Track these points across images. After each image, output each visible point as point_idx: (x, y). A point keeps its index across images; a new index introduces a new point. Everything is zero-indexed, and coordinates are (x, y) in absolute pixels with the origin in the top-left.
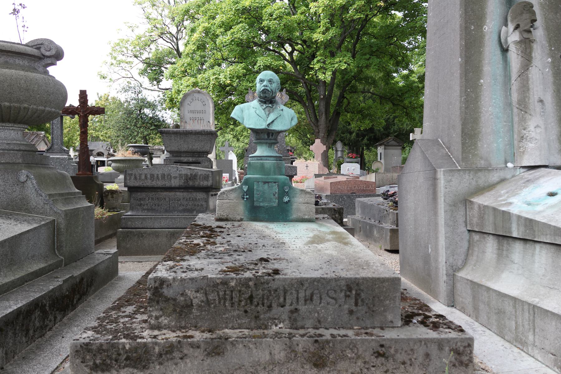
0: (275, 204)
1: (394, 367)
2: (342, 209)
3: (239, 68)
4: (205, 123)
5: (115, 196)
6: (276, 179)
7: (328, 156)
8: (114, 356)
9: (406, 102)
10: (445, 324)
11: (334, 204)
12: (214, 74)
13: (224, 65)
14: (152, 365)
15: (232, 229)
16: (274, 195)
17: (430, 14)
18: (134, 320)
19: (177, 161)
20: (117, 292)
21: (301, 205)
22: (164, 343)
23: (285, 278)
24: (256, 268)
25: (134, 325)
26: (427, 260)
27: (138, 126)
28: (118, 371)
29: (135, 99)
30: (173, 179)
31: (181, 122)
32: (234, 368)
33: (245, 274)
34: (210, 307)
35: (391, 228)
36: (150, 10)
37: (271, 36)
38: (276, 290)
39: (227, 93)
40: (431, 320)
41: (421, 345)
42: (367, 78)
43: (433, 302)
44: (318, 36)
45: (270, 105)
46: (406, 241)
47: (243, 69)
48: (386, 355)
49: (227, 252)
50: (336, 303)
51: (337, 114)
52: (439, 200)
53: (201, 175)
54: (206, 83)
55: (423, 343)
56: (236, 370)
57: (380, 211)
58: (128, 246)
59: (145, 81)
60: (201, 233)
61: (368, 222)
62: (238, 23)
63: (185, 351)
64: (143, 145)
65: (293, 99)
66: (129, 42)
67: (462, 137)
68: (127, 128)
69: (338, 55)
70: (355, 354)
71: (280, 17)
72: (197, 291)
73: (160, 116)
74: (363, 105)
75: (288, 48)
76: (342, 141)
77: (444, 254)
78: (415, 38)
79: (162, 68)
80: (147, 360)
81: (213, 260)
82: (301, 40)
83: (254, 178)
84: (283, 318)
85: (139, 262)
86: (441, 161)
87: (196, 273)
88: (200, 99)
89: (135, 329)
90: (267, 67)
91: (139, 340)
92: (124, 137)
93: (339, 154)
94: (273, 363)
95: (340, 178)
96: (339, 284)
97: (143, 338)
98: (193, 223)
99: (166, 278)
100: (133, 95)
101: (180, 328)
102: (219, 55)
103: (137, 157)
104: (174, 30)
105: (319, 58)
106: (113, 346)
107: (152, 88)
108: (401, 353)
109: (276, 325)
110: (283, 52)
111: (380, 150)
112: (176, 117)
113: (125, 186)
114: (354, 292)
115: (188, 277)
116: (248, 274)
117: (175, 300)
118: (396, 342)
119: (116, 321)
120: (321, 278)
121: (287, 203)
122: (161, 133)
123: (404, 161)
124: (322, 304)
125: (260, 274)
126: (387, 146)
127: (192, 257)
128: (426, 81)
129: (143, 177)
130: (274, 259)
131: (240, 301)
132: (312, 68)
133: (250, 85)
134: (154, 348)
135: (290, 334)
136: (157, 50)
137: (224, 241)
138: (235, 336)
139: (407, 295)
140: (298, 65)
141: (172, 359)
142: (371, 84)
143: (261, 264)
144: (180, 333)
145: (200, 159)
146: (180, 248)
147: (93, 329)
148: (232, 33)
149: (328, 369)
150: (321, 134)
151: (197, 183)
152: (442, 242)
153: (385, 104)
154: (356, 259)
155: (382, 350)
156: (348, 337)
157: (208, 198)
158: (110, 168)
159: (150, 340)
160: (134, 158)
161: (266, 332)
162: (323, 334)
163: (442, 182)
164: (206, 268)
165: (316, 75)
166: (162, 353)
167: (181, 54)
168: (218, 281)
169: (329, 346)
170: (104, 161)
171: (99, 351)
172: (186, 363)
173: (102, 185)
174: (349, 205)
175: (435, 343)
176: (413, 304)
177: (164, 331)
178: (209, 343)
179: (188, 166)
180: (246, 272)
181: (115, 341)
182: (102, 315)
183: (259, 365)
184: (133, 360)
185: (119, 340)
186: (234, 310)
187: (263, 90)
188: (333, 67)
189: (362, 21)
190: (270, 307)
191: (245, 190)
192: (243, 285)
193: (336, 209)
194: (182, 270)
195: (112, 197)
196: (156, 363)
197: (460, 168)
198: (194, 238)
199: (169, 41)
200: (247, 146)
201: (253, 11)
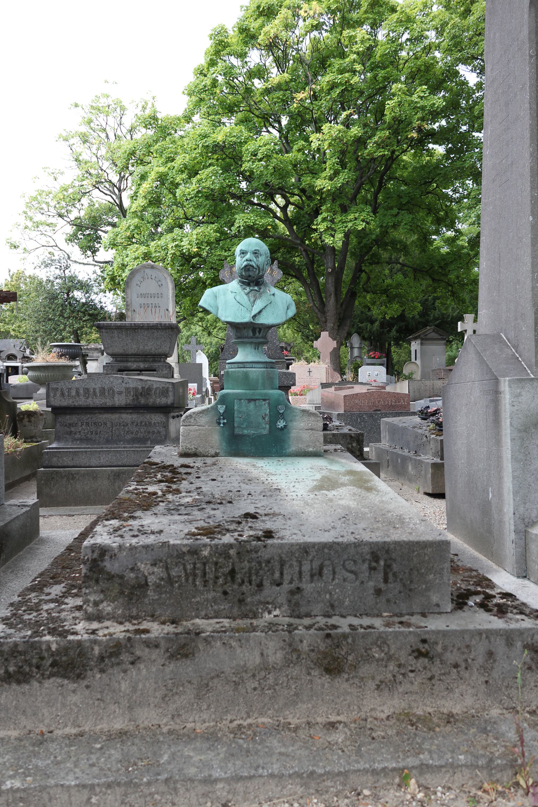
0: (265, 432)
1: (443, 671)
2: (362, 435)
3: (210, 231)
4: (162, 313)
5: (33, 419)
6: (266, 394)
7: (339, 356)
8: (34, 661)
9: (452, 276)
10: (516, 608)
11: (350, 427)
12: (174, 240)
13: (188, 228)
14: (89, 673)
15: (203, 469)
17: (486, 152)
18: (63, 606)
19: (122, 368)
20: (38, 563)
22: (107, 641)
23: (282, 544)
24: (239, 529)
25: (63, 614)
26: (486, 509)
27: (65, 315)
28: (40, 682)
29: (61, 278)
30: (116, 395)
31: (127, 310)
32: (209, 677)
33: (223, 538)
34: (173, 587)
35: (433, 461)
36: (79, 147)
37: (255, 184)
38: (268, 562)
39: (193, 266)
40: (495, 601)
41: (481, 639)
42: (394, 243)
43: (496, 571)
44: (322, 183)
45: (256, 288)
46: (455, 481)
47: (216, 231)
48: (431, 655)
49: (196, 505)
50: (357, 579)
51: (352, 295)
52: (503, 424)
53: (157, 389)
55: (484, 636)
56: (212, 678)
57: (416, 437)
58: (53, 492)
59: (75, 251)
60: (159, 476)
61: (400, 452)
62: (205, 167)
63: (138, 653)
64: (73, 343)
65: (289, 274)
66: (51, 195)
67: (535, 331)
68: (50, 320)
69: (352, 209)
70: (386, 654)
71: (268, 157)
72: (154, 565)
73: (96, 301)
74: (389, 281)
75: (279, 199)
76: (359, 334)
77: (512, 502)
78: (463, 184)
79: (99, 232)
80: (83, 667)
81: (177, 517)
82: (299, 189)
83: (233, 394)
84: (279, 601)
85: (70, 515)
86: (505, 366)
87: (152, 537)
89: (65, 620)
90: (249, 231)
91: (71, 637)
92: (45, 331)
93: (356, 352)
94: (265, 667)
95: (358, 389)
96: (360, 551)
97: (76, 633)
98: (146, 460)
99: (109, 546)
100: (58, 272)
101: (130, 618)
102: (180, 213)
103: (64, 362)
104: (115, 179)
105: (325, 215)
106: (33, 646)
107: (85, 261)
108: (451, 651)
109: (270, 613)
110: (273, 206)
111: (415, 346)
112: (119, 301)
113: (48, 406)
114: (382, 563)
115: (141, 543)
116: (227, 539)
117: (122, 577)
118: (444, 635)
119: (37, 608)
120: (334, 543)
121: (282, 429)
122: (100, 328)
123: (451, 361)
124: (337, 581)
125: (244, 538)
126: (424, 340)
128: (481, 244)
129: (73, 393)
130: (266, 515)
131: (217, 578)
132: (316, 230)
133: (226, 254)
134: (93, 649)
135: (290, 625)
136: (91, 205)
138: (210, 629)
139: (460, 564)
140: (295, 224)
141: (118, 664)
142: (401, 250)
143: (247, 522)
144: (130, 625)
145: (156, 365)
146: (130, 500)
147: (3, 620)
148: (199, 181)
149: (346, 676)
150: (330, 325)
151: (151, 400)
152: (508, 483)
153: (421, 279)
154: (383, 512)
155: (424, 648)
156: (374, 628)
157: (168, 421)
158: (26, 377)
159: (86, 636)
160: (60, 364)
161: (255, 622)
162: (337, 624)
163: (508, 396)
164: (167, 529)
165: (320, 238)
166: (104, 655)
167: (126, 211)
168: (185, 549)
169: (348, 643)
170: (17, 367)
171: (12, 654)
172: (139, 669)
173: (15, 404)
174: (372, 428)
175: (501, 635)
176: (468, 577)
177: (107, 623)
178: (173, 640)
179: (139, 375)
180: (225, 535)
181: (36, 639)
182: (16, 599)
183: (246, 671)
184: (61, 666)
185: (41, 637)
186: (208, 591)
187: (245, 266)
189: (387, 160)
190: (260, 586)
191: (222, 411)
192: (220, 555)
193: (353, 435)
194: (132, 533)
195: (30, 421)
196: (96, 670)
197: (533, 376)
198: (149, 483)
199: (108, 193)
201: (229, 148)
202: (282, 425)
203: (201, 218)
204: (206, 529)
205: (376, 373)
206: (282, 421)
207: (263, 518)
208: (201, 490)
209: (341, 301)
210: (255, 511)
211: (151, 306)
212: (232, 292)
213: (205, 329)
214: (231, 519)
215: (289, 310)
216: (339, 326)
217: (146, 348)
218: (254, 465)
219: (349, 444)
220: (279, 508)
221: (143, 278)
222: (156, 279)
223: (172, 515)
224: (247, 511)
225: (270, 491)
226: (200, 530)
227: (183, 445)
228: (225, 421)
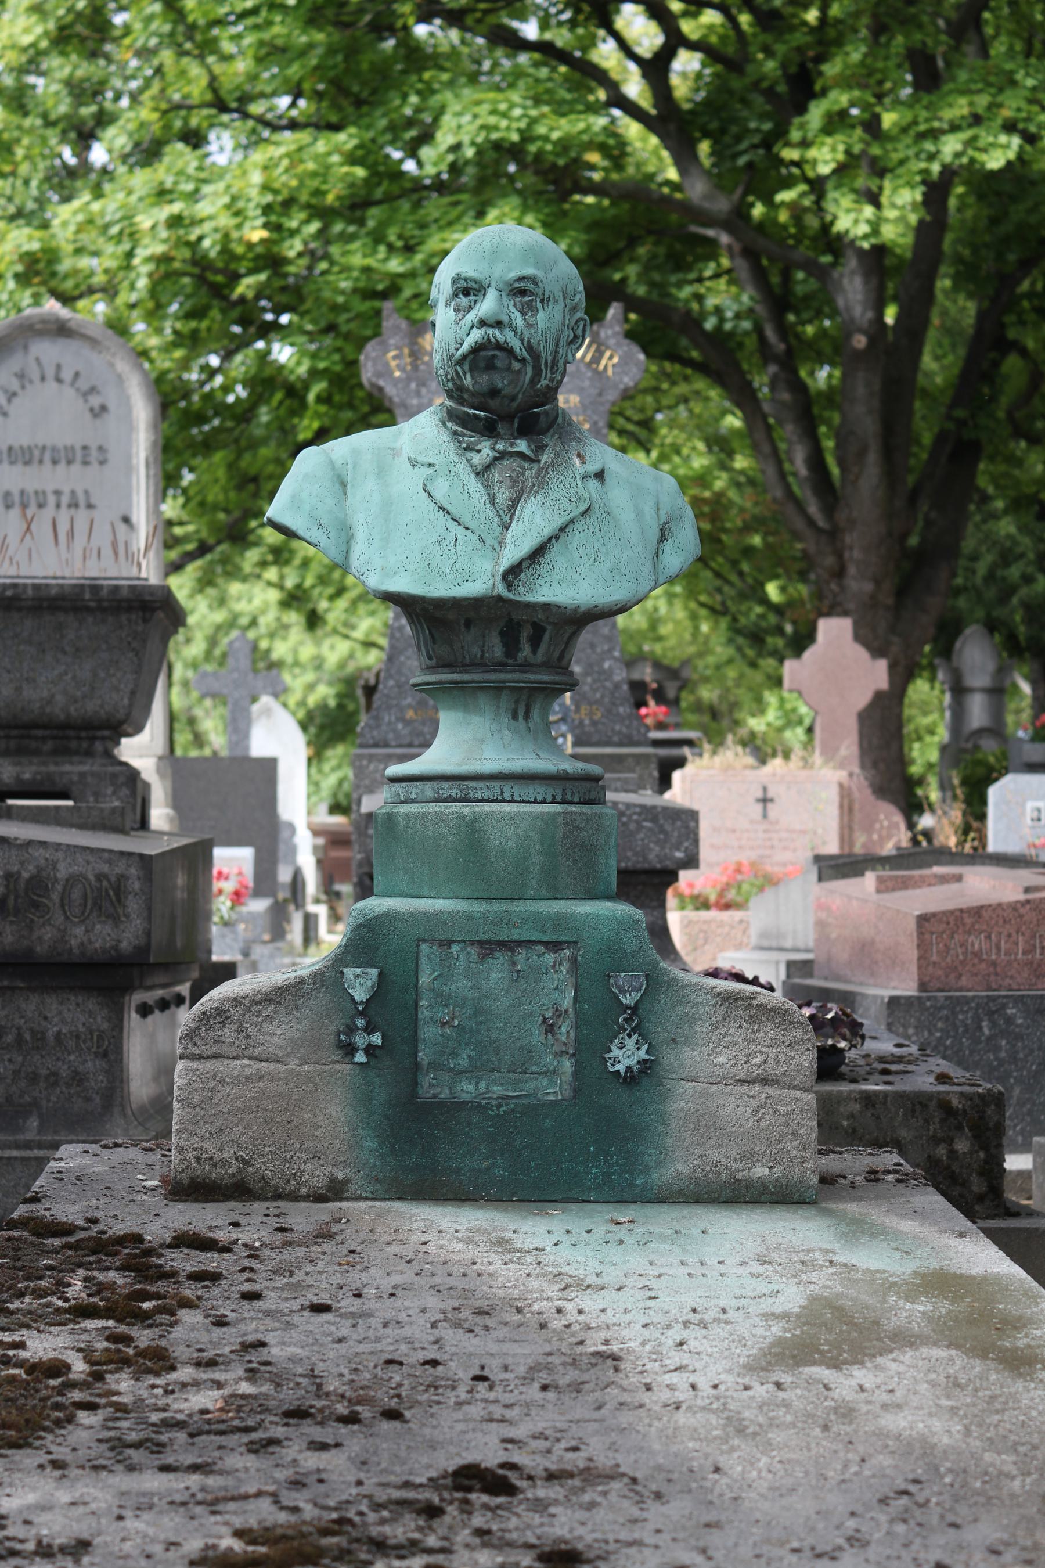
2: (998, 1101)
4: (102, 538)
6: (559, 921)
12: (163, 194)
13: (222, 146)
16: (550, 1029)
21: (732, 1090)
24: (432, 1541)
45: (522, 446)
47: (352, 159)
51: (960, 452)
53: (72, 881)
54: (110, 257)
60: (76, 1289)
69: (963, 76)
75: (637, 26)
81: (153, 1482)
83: (414, 917)
88: (67, 375)
95: (983, 886)
98: (21, 1211)
102: (194, 81)
105: (840, 98)
110: (606, 54)
121: (631, 1079)
127: (16, 1454)
130: (551, 1477)
133: (395, 265)
137: (226, 1341)
145: (71, 769)
150: (858, 585)
151: (48, 934)
188: (932, 157)
191: (360, 995)
198: (32, 1320)
200: (373, 658)
202: (632, 1062)
203: (284, 101)
204: (284, 1537)
206: (630, 1043)
207: (541, 1493)
208: (263, 1354)
209: (911, 480)
210: (502, 1457)
211: (51, 500)
212: (414, 463)
213: (294, 599)
214: (397, 1494)
215: (668, 546)
216: (902, 592)
217: (28, 693)
218: (502, 1242)
219: (936, 1141)
220: (613, 1447)
221: (21, 376)
223: (131, 1468)
224: (469, 1457)
225: (574, 1363)
226: (253, 1542)
227: (187, 1144)
228: (377, 1039)
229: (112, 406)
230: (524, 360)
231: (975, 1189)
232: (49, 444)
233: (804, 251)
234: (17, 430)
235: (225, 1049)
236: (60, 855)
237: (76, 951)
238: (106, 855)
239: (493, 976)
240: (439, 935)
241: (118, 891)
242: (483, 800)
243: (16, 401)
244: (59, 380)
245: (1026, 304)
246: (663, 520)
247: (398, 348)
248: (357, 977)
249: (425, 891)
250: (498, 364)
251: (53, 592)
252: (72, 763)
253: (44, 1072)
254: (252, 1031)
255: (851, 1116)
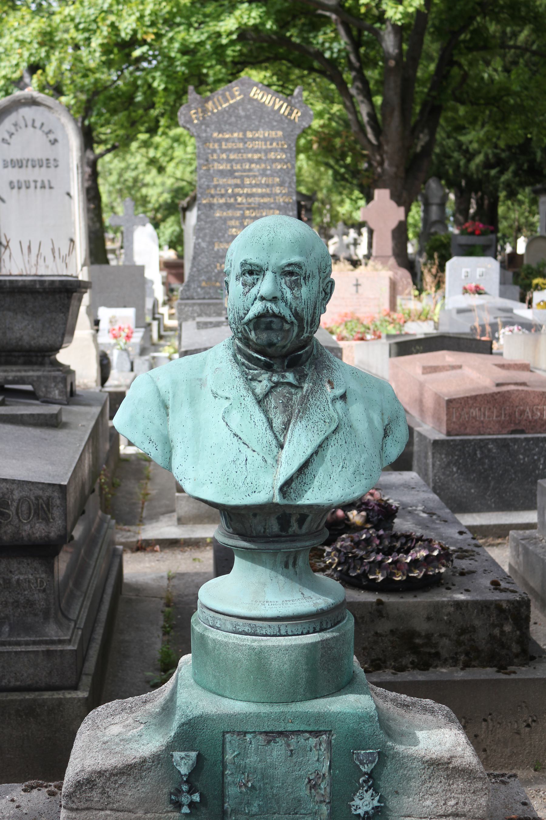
6: (319, 717)
45: (290, 377)
53: (21, 500)
88: (38, 124)
151: (10, 529)
187: (259, 317)
191: (184, 770)
205: (479, 271)
206: (367, 796)
211: (32, 185)
215: (389, 440)
219: (494, 626)
221: (15, 125)
222: (45, 129)
228: (196, 798)
229: (60, 139)
230: (292, 323)
231: (514, 650)
232: (30, 158)
233: (368, 22)
234: (15, 151)
235: (94, 805)
236: (15, 486)
237: (26, 539)
238: (41, 486)
239: (275, 753)
240: (237, 728)
241: (48, 505)
242: (266, 635)
243: (13, 137)
244: (34, 127)
245: (462, 45)
246: (386, 423)
247: (196, 109)
248: (182, 758)
249: (227, 693)
250: (274, 326)
251: (20, 284)
252: (33, 371)
253: (11, 600)
254: (111, 793)
255: (449, 614)
